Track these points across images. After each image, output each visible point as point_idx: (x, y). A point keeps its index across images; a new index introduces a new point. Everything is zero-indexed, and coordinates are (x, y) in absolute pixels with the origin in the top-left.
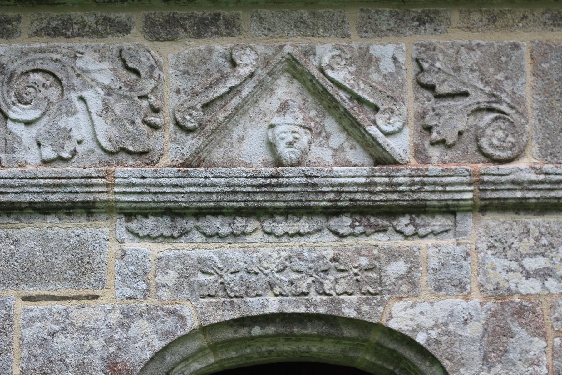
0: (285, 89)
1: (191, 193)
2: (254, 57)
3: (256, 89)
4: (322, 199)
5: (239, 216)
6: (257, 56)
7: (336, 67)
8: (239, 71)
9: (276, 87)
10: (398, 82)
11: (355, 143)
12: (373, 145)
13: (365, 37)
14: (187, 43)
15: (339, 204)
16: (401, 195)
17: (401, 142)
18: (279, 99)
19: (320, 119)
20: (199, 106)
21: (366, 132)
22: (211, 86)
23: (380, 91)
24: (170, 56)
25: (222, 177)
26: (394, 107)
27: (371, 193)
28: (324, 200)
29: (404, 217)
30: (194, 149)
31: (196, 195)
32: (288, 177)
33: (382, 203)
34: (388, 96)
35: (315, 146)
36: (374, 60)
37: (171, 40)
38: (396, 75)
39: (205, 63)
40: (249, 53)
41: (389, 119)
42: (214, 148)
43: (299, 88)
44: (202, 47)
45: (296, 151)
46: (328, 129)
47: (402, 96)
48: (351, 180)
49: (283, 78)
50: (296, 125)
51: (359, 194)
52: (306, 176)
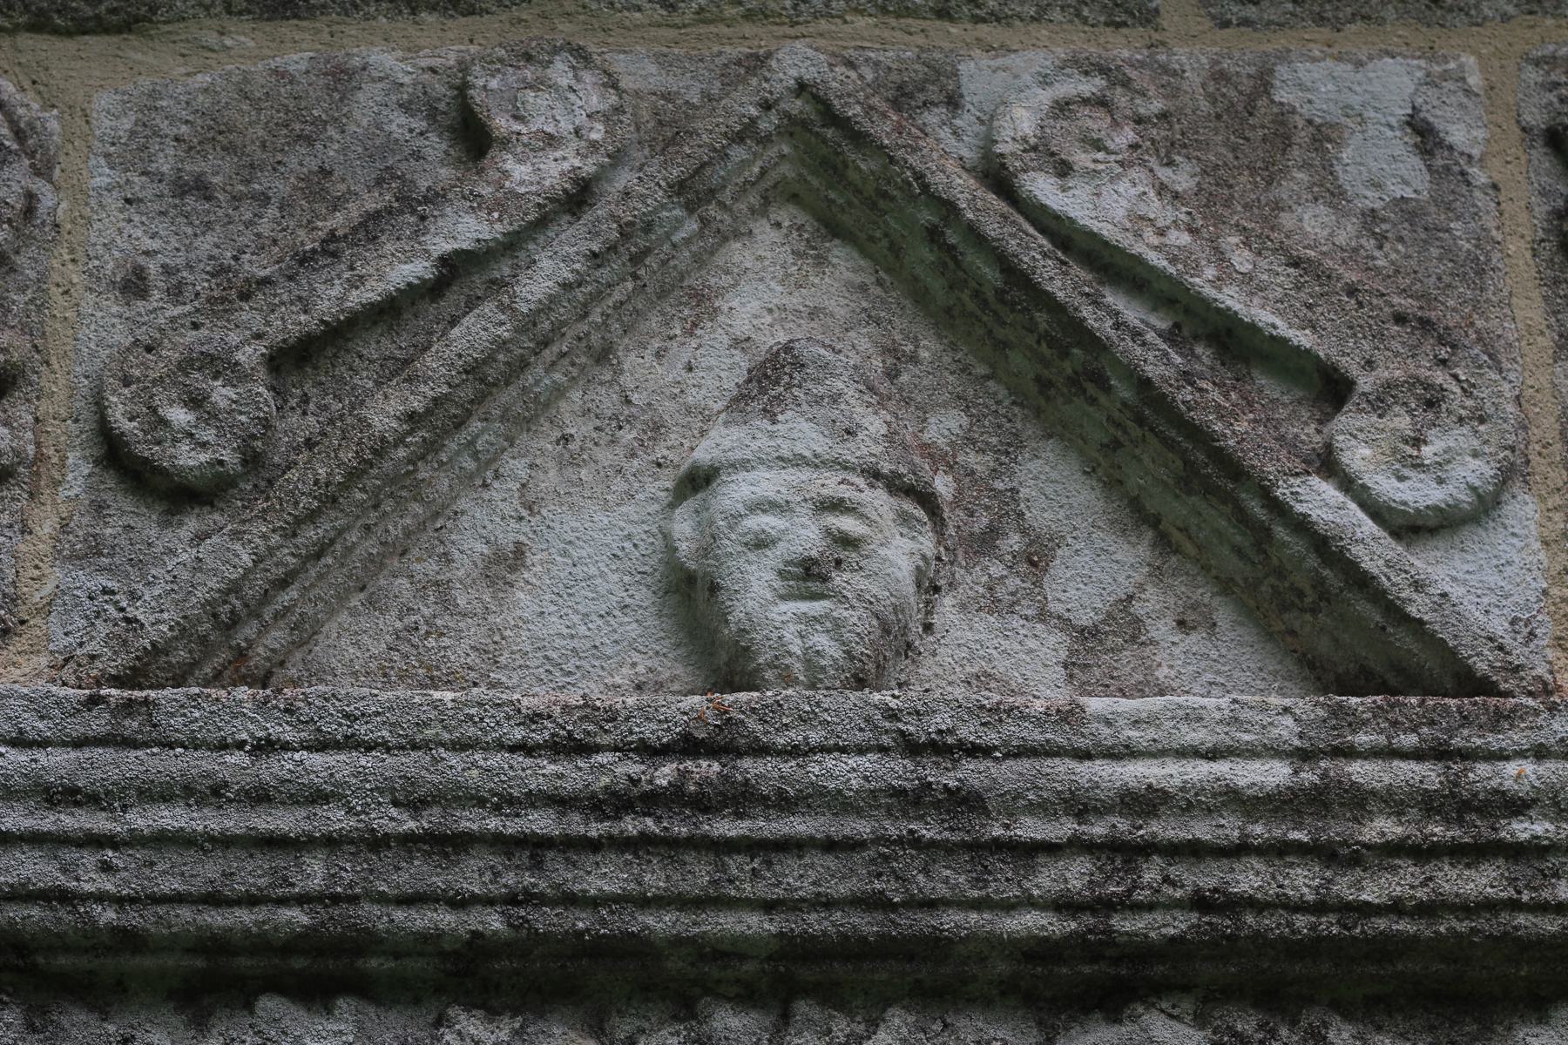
0: (776, 294)
1: (162, 840)
2: (594, 99)
3: (604, 274)
4: (1013, 892)
5: (469, 1007)
6: (613, 99)
7: (1082, 159)
8: (506, 174)
9: (726, 280)
10: (1448, 253)
11: (1204, 594)
12: (1324, 595)
13: (1246, 22)
14: (211, 38)
15: (1125, 924)
16: (1521, 870)
17: (1493, 579)
18: (740, 343)
19: (989, 458)
20: (249, 355)
21: (1279, 509)
22: (331, 247)
23: (1352, 291)
24: (104, 101)
25: (369, 747)
26: (1440, 377)
27: (1325, 854)
28: (1030, 903)
29: (1543, 1020)
30: (201, 594)
31: (191, 855)
32: (793, 751)
33: (1404, 926)
34: (1400, 319)
35: (963, 607)
36: (1303, 136)
37: (118, 30)
38: (1436, 216)
39: (309, 140)
40: (564, 81)
41: (1417, 442)
42: (332, 613)
43: (863, 288)
44: (296, 61)
45: (841, 612)
46: (1041, 516)
47: (1480, 323)
48: (1200, 771)
49: (764, 232)
50: (845, 467)
51: (1256, 863)
52: (912, 748)
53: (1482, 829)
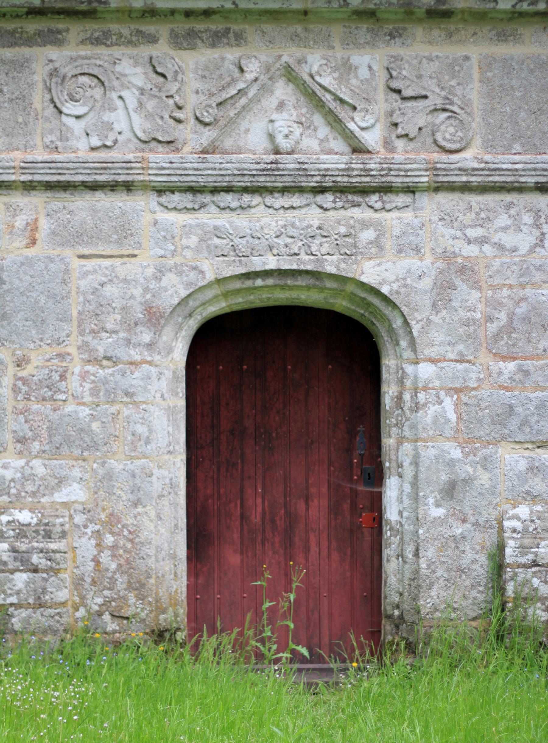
1: (209, 175)
2: (258, 65)
7: (323, 74)
10: (372, 86)
11: (337, 135)
15: (324, 184)
16: (372, 178)
18: (277, 98)
20: (214, 105)
21: (346, 127)
22: (224, 88)
24: (191, 63)
26: (368, 107)
27: (349, 176)
36: (353, 68)
38: (371, 81)
46: (316, 124)
52: (299, 163)
53: (367, 173)
